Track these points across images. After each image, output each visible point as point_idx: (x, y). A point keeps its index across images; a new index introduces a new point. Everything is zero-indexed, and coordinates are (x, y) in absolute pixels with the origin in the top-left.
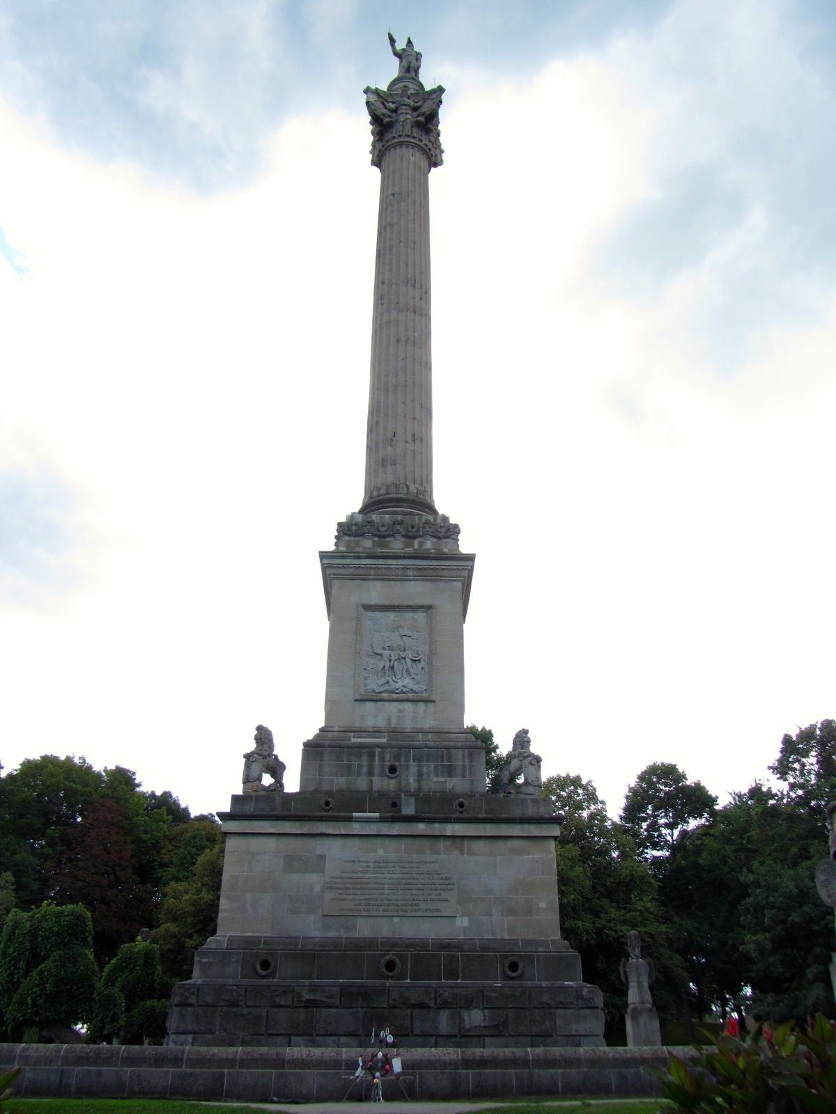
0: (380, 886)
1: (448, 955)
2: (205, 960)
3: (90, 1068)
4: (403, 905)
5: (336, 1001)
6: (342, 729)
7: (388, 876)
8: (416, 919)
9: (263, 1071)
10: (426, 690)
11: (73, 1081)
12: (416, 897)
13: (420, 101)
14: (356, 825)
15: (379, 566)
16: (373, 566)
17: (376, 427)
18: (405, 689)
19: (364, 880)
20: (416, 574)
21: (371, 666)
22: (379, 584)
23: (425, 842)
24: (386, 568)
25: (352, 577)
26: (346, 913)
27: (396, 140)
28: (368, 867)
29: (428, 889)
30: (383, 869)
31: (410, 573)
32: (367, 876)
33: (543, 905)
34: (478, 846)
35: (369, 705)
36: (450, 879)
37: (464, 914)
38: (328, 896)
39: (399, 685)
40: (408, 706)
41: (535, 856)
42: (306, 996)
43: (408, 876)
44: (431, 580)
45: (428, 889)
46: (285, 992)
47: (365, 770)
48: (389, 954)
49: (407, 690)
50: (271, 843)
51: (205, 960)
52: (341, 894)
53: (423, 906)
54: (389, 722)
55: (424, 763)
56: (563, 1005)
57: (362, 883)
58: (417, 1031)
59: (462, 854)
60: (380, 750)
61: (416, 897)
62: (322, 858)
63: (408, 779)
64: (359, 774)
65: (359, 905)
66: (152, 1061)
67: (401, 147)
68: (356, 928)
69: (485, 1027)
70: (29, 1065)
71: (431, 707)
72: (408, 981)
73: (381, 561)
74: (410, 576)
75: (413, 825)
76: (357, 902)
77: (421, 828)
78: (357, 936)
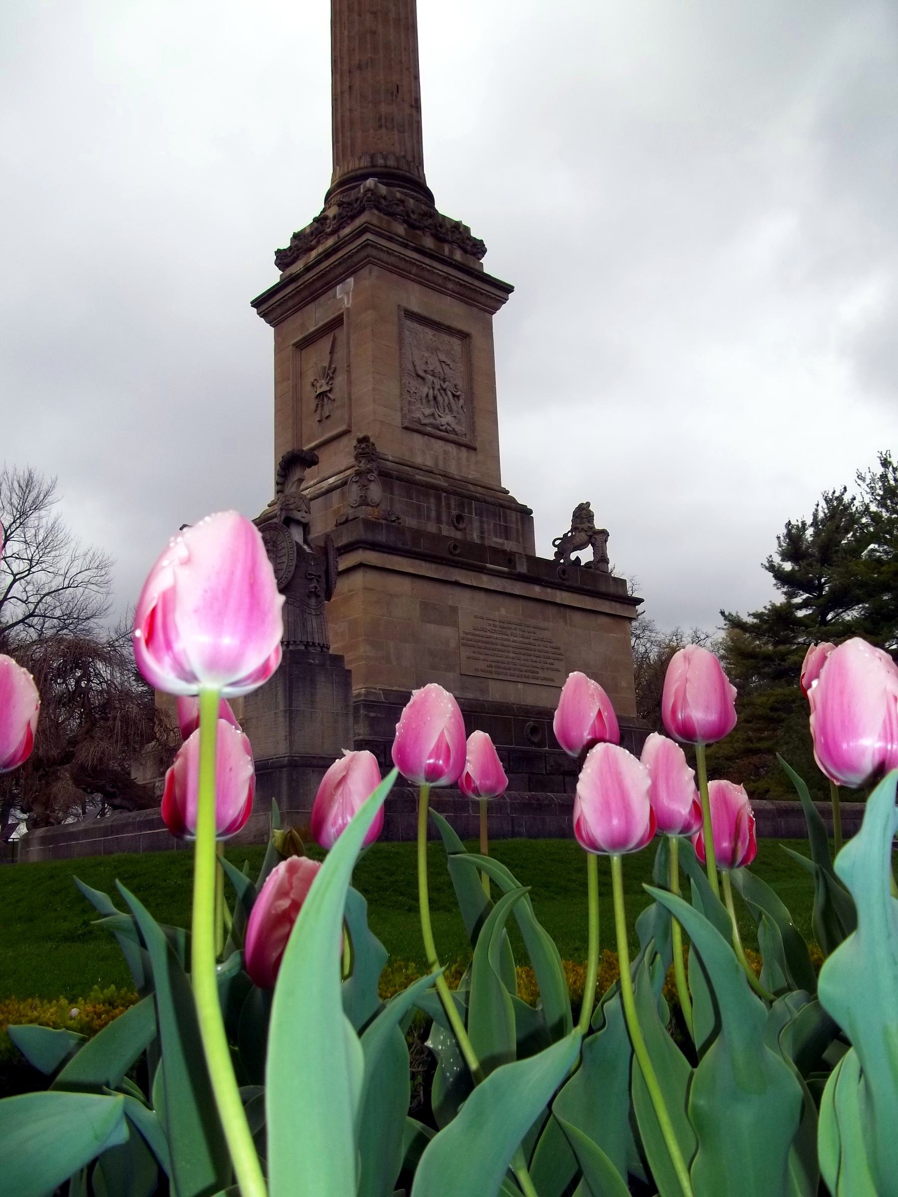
2: (372, 715)
4: (526, 671)
6: (397, 460)
7: (512, 638)
8: (501, 682)
10: (465, 434)
12: (535, 664)
14: (485, 578)
15: (424, 266)
16: (418, 263)
18: (449, 428)
20: (456, 290)
23: (538, 607)
24: (430, 271)
29: (544, 657)
30: (508, 631)
31: (450, 286)
32: (495, 636)
33: (624, 684)
34: (577, 617)
35: (417, 437)
36: (559, 649)
38: (465, 653)
44: (466, 303)
45: (544, 657)
47: (433, 514)
48: (530, 721)
49: (451, 429)
50: (404, 586)
51: (372, 715)
52: (475, 653)
60: (445, 494)
61: (535, 664)
62: (454, 610)
63: (472, 534)
64: (429, 518)
65: (491, 666)
71: (472, 453)
72: (547, 748)
73: (427, 261)
74: (448, 290)
76: (489, 663)
77: (537, 591)
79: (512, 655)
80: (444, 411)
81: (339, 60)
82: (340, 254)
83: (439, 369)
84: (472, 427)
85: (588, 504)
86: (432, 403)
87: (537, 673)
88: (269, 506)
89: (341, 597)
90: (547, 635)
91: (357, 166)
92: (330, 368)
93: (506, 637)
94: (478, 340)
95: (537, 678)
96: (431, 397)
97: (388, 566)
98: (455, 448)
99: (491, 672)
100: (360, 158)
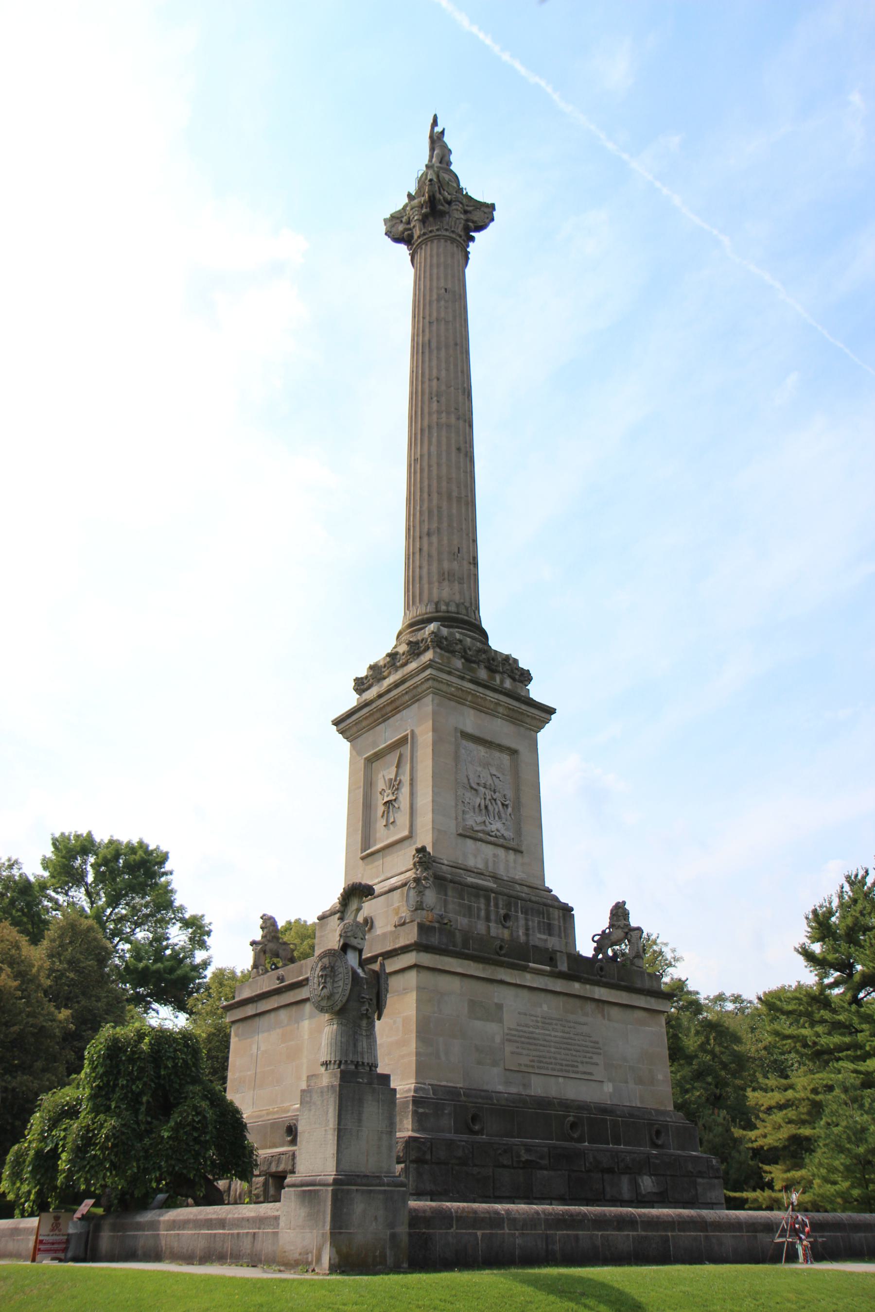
0: (548, 1043)
1: (612, 1120)
3: (569, 1232)
5: (544, 1162)
6: (451, 864)
7: (553, 1033)
9: (695, 1234)
11: (557, 1247)
13: (471, 206)
14: (528, 976)
16: (473, 692)
18: (498, 834)
19: (534, 1035)
20: (505, 713)
21: (467, 800)
22: (472, 712)
23: (577, 1002)
25: (451, 697)
26: (523, 1069)
27: (433, 234)
28: (537, 1021)
29: (583, 1051)
31: (501, 710)
32: (537, 1031)
34: (615, 1012)
36: (597, 1043)
37: (610, 1080)
38: (509, 1048)
39: (494, 827)
40: (501, 852)
42: (525, 1157)
43: (567, 1035)
45: (583, 1051)
46: (505, 1151)
47: (483, 913)
50: (455, 984)
53: (581, 1068)
55: (529, 917)
56: (701, 1174)
57: (535, 1039)
58: (608, 1197)
62: (499, 1007)
66: (615, 1224)
67: (452, 243)
69: (655, 1193)
70: (517, 1230)
71: (519, 856)
72: (586, 1144)
73: (481, 689)
75: (571, 983)
76: (531, 1058)
77: (576, 987)
78: (533, 1094)
79: (553, 1050)
83: (490, 782)
84: (519, 832)
85: (624, 903)
91: (424, 611)
92: (395, 780)
95: (577, 1072)
96: (483, 807)
99: (533, 1067)
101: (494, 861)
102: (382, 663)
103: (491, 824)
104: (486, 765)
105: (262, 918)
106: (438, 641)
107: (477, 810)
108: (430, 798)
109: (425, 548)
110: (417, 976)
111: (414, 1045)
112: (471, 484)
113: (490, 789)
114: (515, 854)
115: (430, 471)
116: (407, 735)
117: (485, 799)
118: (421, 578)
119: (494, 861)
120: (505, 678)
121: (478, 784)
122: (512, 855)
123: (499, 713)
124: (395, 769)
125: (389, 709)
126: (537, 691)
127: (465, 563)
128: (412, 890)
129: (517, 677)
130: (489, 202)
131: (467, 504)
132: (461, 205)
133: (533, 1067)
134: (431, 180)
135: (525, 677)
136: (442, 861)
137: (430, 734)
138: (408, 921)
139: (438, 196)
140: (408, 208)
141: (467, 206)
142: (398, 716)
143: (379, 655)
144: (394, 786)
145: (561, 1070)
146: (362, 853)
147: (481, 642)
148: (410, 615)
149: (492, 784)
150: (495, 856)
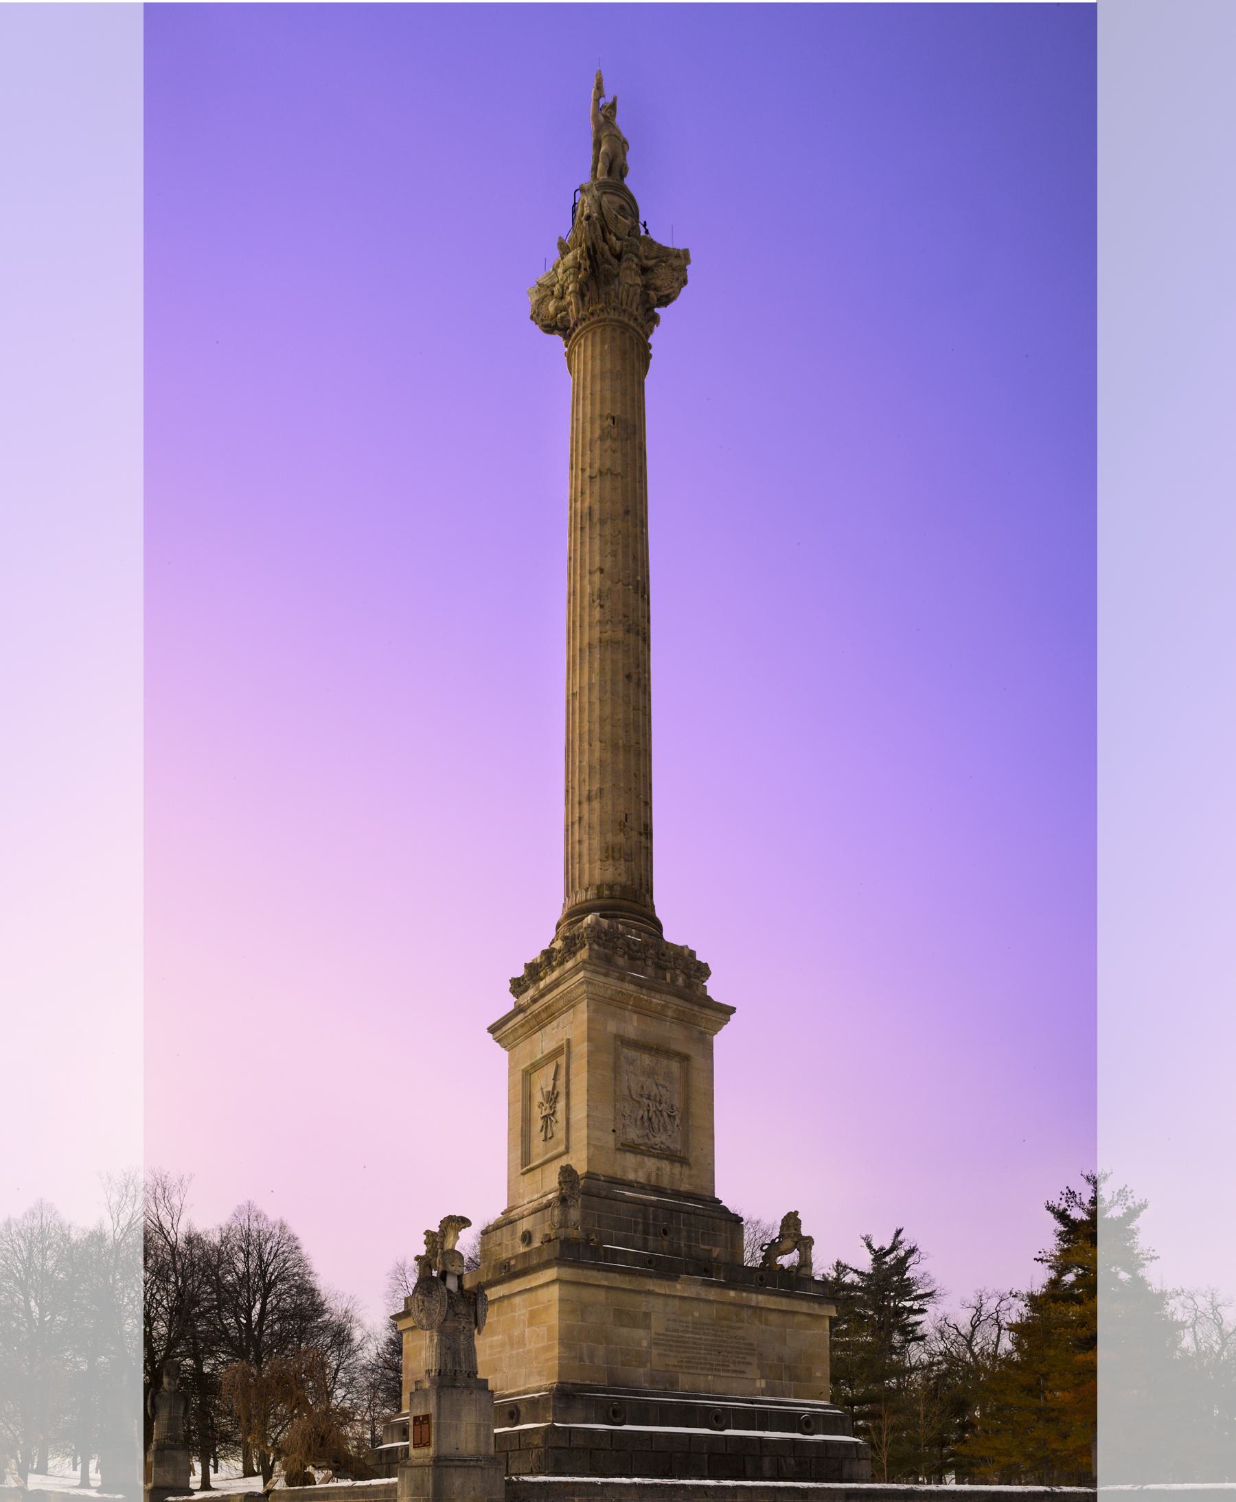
7: (704, 1337)
17: (572, 827)
32: (687, 1335)
36: (751, 1344)
39: (657, 1140)
41: (815, 1332)
47: (640, 1227)
50: (601, 1295)
53: (732, 1367)
54: (649, 1180)
59: (761, 1324)
60: (653, 1208)
62: (647, 1315)
68: (678, 1382)
79: (703, 1351)
80: (659, 1131)
81: (570, 790)
82: (561, 988)
83: (655, 1091)
84: (686, 1142)
85: (796, 1213)
86: (646, 1124)
87: (728, 1366)
88: (502, 1214)
89: (542, 1305)
90: (740, 1333)
92: (553, 1093)
93: (699, 1336)
94: (697, 1061)
95: (729, 1371)
96: (645, 1118)
97: (582, 1281)
98: (668, 1164)
99: (681, 1367)
100: (587, 890)
101: (657, 1174)
102: (539, 961)
103: (655, 1137)
104: (651, 1073)
105: (425, 1234)
106: (597, 935)
107: (639, 1123)
108: (585, 1114)
109: (586, 816)
110: (560, 1289)
111: (557, 1351)
112: (644, 725)
113: (655, 1100)
114: (682, 1166)
115: (591, 711)
116: (563, 1044)
117: (648, 1111)
118: (580, 856)
119: (657, 1174)
120: (678, 975)
121: (641, 1096)
122: (677, 1169)
123: (667, 1016)
124: (552, 1081)
125: (544, 1016)
126: (715, 989)
127: (634, 834)
128: (556, 1208)
129: (692, 973)
130: (680, 246)
131: (638, 755)
132: (636, 260)
133: (681, 1367)
134: (588, 218)
135: (703, 971)
136: (597, 1177)
137: (586, 1044)
138: (552, 1238)
139: (601, 244)
140: (560, 270)
141: (647, 258)
142: (554, 1023)
143: (534, 954)
144: (551, 1100)
145: (712, 1369)
146: (522, 1168)
147: (650, 934)
148: (570, 904)
149: (658, 1094)
150: (658, 1169)
